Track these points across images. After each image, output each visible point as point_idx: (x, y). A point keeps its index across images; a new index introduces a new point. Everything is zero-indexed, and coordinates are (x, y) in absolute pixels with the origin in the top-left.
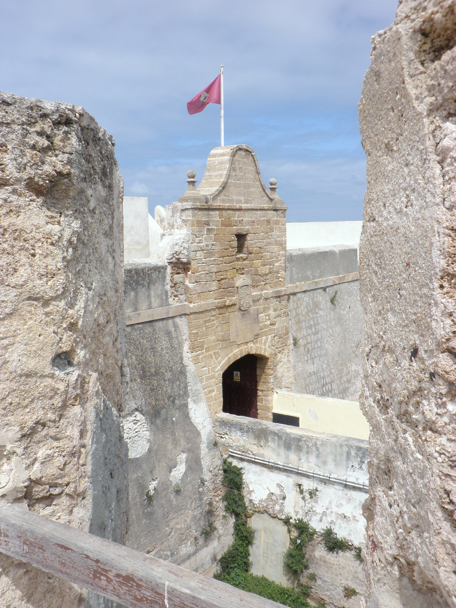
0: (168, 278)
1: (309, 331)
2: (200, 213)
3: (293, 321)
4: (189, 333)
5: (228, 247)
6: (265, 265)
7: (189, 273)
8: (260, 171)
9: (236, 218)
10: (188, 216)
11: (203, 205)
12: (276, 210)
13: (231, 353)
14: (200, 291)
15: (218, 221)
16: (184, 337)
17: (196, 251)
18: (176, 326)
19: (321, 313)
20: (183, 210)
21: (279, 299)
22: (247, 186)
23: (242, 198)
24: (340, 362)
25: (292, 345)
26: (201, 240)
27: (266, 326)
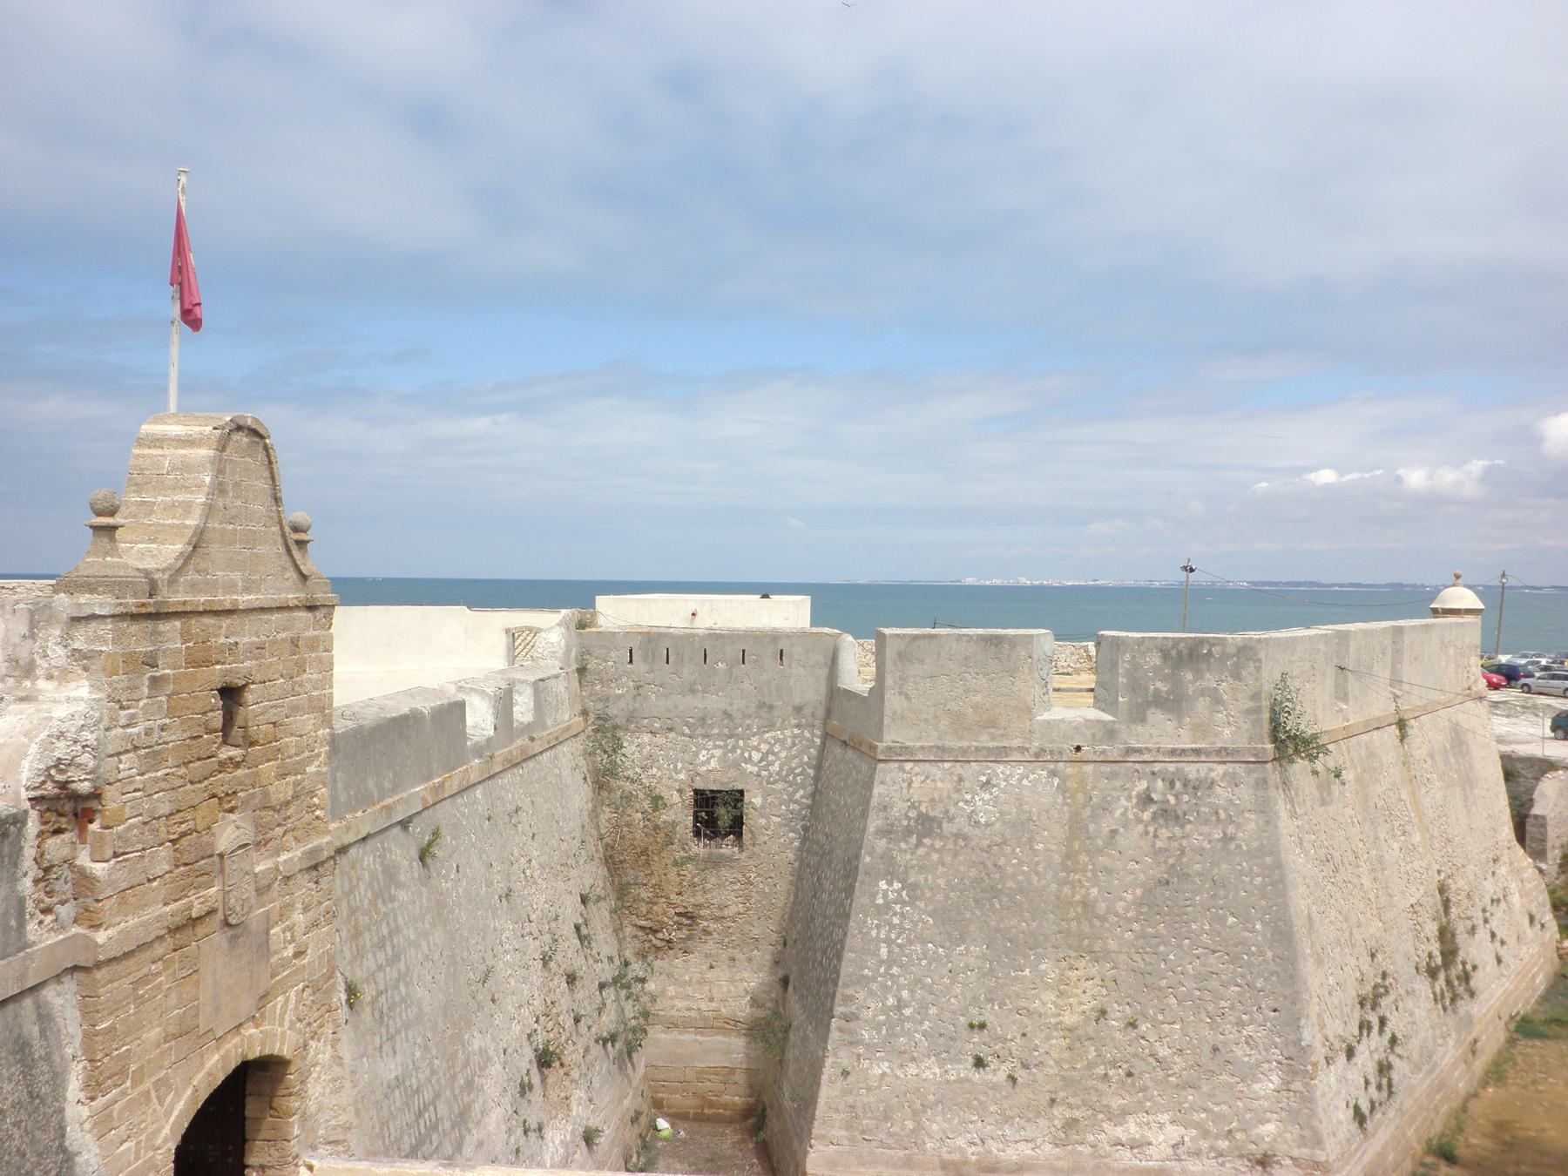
0: (29, 852)
1: (381, 956)
2: (134, 628)
3: (344, 934)
4: (86, 1035)
5: (201, 731)
6: (283, 776)
7: (94, 827)
8: (284, 495)
9: (222, 640)
10: (101, 639)
11: (143, 605)
12: (311, 608)
13: (198, 1071)
14: (124, 885)
15: (179, 651)
16: (69, 1051)
17: (120, 753)
18: (45, 1018)
19: (402, 895)
20: (76, 620)
21: (315, 873)
22: (251, 540)
23: (237, 576)
24: (449, 1032)
25: (346, 1008)
26: (133, 716)
27: (285, 963)
